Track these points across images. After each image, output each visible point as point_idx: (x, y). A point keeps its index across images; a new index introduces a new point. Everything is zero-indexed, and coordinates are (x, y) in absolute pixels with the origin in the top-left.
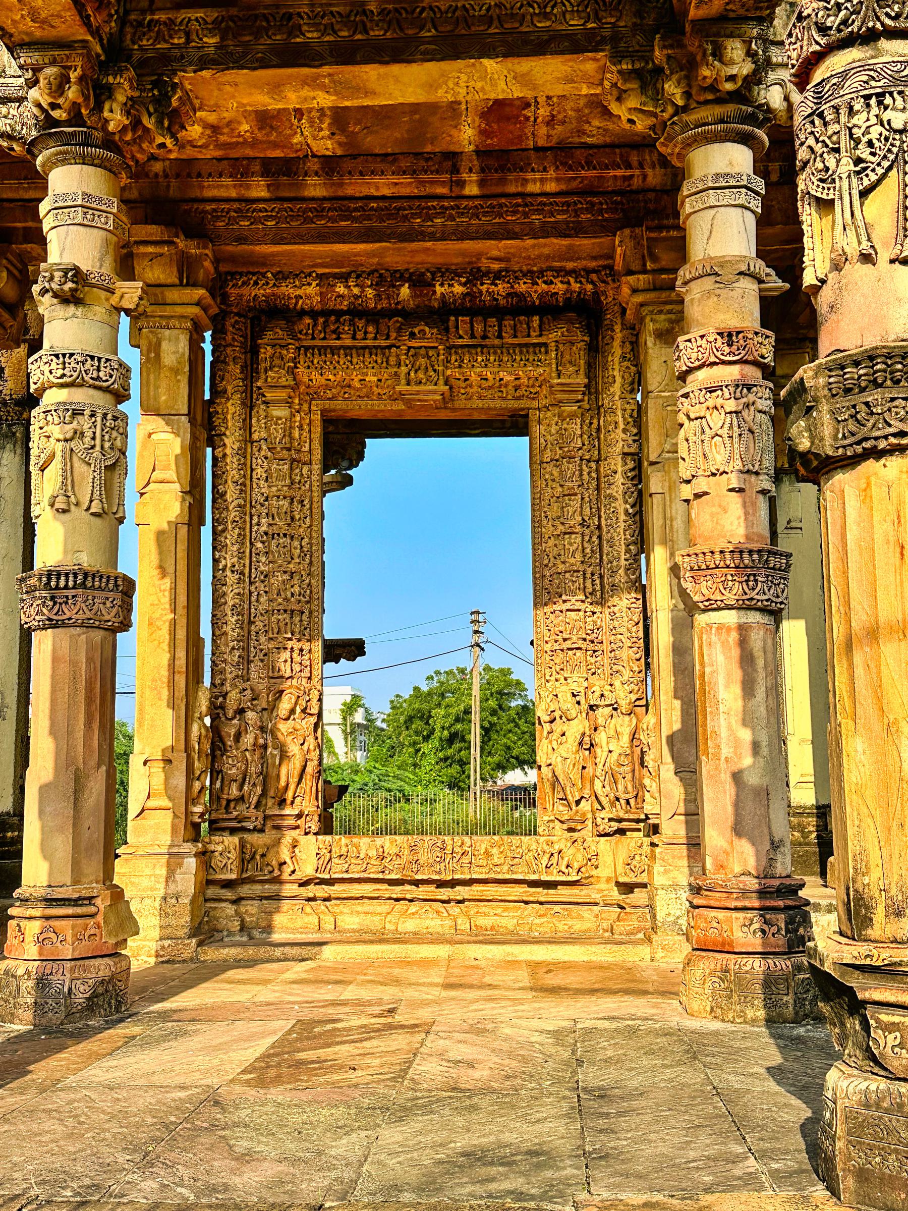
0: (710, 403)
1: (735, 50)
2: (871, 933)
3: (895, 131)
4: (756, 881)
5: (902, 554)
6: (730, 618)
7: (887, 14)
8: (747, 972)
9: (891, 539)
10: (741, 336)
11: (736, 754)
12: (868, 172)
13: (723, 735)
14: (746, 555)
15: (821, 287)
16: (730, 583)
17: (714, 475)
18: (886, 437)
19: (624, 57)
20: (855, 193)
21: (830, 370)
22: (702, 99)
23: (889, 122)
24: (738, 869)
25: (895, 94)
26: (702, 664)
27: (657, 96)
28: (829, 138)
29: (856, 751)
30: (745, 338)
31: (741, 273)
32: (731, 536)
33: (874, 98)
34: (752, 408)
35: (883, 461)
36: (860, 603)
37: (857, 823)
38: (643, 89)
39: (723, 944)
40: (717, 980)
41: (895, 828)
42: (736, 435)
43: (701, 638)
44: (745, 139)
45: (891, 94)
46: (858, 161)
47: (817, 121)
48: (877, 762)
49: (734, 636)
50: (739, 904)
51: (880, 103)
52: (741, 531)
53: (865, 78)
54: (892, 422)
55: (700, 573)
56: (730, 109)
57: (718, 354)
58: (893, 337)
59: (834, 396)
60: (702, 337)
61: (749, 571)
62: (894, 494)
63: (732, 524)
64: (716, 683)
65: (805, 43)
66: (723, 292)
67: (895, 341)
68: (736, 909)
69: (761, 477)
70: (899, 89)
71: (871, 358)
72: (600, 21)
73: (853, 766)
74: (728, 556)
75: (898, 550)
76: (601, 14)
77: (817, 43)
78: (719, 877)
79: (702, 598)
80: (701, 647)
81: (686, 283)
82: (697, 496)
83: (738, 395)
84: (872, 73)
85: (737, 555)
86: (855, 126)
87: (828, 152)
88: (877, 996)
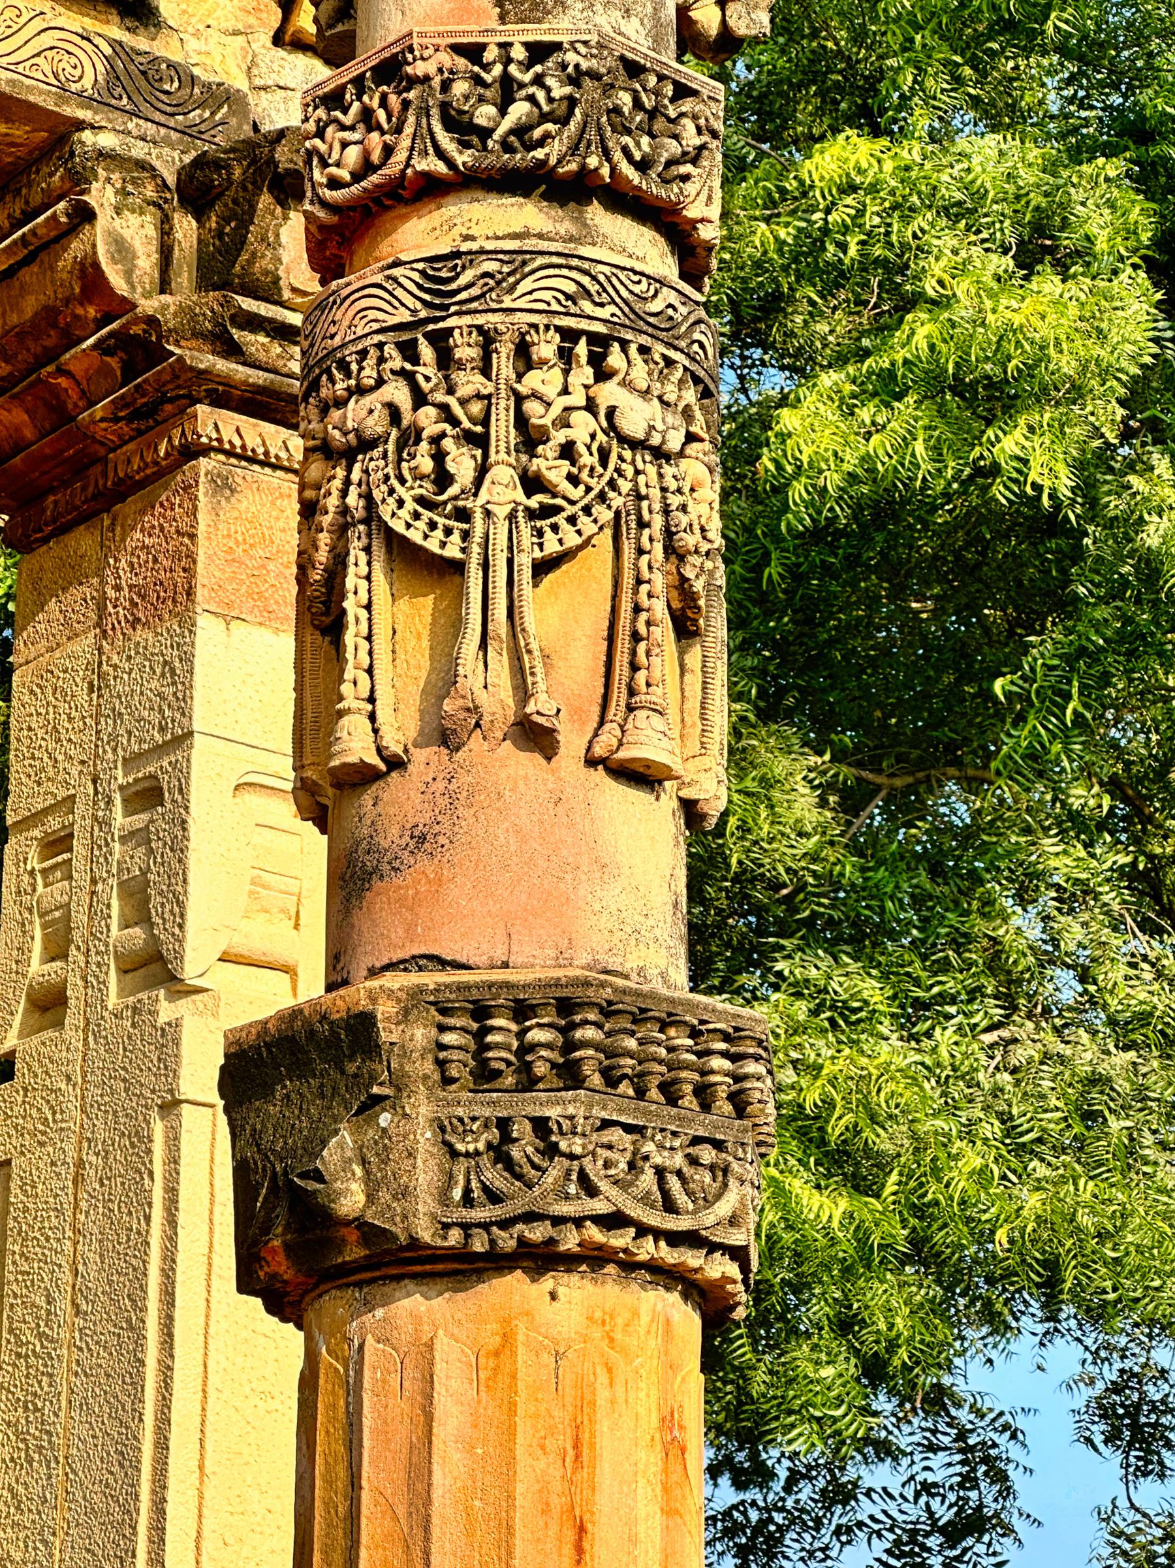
3: (623, 440)
5: (579, 1550)
7: (626, 151)
9: (555, 1501)
12: (560, 519)
18: (578, 1222)
20: (524, 562)
21: (444, 1012)
23: (611, 412)
25: (633, 349)
28: (463, 402)
33: (583, 341)
35: (547, 1283)
45: (624, 344)
46: (532, 483)
47: (426, 352)
51: (597, 361)
53: (571, 288)
54: (603, 1186)
58: (584, 958)
59: (447, 1081)
62: (567, 1379)
65: (406, 143)
67: (588, 967)
70: (644, 340)
71: (566, 1007)
75: (570, 1535)
77: (441, 154)
84: (585, 280)
86: (535, 395)
87: (456, 438)
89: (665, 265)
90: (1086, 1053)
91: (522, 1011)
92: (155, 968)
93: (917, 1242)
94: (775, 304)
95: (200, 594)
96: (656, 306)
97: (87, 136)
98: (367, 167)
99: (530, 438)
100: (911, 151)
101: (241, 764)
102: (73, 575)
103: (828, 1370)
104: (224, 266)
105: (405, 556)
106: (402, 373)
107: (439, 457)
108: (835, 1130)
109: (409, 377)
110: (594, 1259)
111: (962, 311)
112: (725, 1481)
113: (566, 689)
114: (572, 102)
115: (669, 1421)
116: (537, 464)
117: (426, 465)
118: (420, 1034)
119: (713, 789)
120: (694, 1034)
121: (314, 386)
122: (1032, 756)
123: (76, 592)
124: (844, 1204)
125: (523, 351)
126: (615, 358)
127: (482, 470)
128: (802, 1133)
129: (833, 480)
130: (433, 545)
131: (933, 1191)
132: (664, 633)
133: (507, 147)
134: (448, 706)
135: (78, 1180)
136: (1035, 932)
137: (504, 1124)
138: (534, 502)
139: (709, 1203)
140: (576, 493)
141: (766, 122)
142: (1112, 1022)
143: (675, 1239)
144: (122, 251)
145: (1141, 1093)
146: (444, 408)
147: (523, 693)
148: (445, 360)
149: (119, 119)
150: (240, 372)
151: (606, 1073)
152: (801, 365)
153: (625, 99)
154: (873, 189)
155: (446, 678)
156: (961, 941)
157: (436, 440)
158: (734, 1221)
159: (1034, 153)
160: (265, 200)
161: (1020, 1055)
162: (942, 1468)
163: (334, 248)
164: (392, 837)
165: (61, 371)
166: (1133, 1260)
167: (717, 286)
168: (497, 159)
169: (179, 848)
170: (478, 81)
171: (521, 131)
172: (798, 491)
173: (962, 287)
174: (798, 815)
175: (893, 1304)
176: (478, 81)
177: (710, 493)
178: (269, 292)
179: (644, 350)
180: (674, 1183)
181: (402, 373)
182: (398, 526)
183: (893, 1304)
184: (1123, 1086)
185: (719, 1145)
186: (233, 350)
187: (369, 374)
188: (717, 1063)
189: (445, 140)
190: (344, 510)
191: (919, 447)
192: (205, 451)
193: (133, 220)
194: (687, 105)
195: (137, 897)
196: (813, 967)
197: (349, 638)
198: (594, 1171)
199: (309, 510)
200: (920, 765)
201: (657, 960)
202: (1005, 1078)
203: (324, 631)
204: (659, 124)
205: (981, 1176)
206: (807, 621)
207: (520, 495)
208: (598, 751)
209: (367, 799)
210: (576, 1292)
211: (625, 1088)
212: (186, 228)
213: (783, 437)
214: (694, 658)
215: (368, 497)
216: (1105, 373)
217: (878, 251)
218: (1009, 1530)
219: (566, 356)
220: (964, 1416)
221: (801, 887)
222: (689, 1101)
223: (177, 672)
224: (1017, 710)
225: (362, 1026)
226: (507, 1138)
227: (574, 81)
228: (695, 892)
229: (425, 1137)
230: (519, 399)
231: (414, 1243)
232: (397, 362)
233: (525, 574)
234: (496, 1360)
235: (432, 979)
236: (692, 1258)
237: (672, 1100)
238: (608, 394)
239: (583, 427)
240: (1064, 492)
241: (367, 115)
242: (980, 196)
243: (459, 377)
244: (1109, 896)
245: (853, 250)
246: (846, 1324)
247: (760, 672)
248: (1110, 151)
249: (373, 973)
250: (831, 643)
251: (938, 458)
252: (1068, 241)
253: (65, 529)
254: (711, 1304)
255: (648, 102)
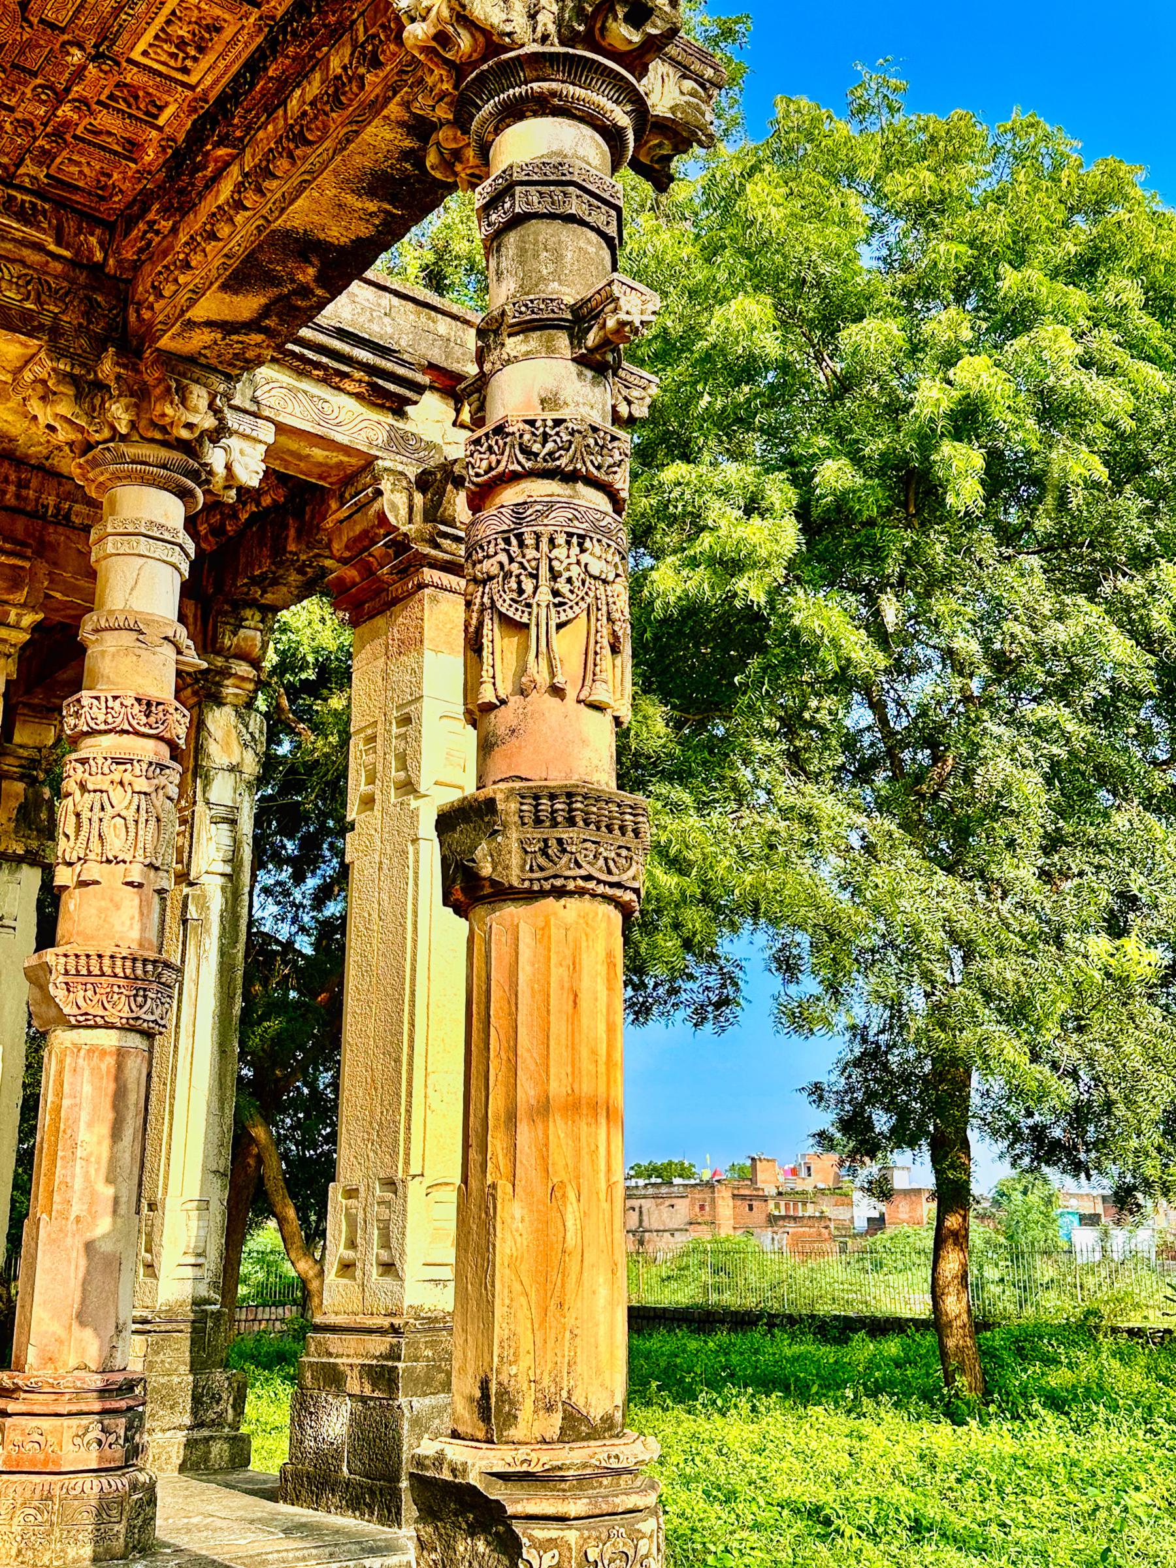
0: (116, 777)
1: (199, 396)
2: (513, 1433)
4: (99, 1377)
5: (575, 1003)
6: (109, 1039)
8: (75, 1498)
10: (161, 708)
11: (89, 1212)
13: (76, 1187)
14: (139, 965)
15: (496, 707)
16: (116, 997)
17: (109, 861)
18: (574, 878)
19: (63, 356)
20: (553, 624)
22: (149, 435)
24: (73, 1362)
26: (59, 1094)
27: (93, 413)
29: (513, 1218)
30: (165, 712)
31: (166, 638)
32: (121, 938)
34: (161, 792)
35: (563, 901)
36: (529, 1050)
37: (507, 1302)
38: (78, 398)
39: (46, 1462)
40: (33, 1511)
41: (552, 1307)
42: (142, 820)
43: (61, 1062)
44: (184, 494)
46: (556, 593)
47: (514, 541)
48: (537, 1230)
49: (111, 1061)
50: (74, 1408)
51: (580, 545)
52: (135, 934)
55: (80, 979)
56: (176, 456)
57: (134, 723)
58: (576, 777)
59: (524, 824)
60: (115, 698)
61: (139, 984)
62: (570, 938)
63: (123, 924)
64: (77, 1121)
65: (505, 458)
66: (143, 653)
68: (70, 1414)
69: (161, 873)
71: (569, 795)
72: (42, 304)
73: (508, 1236)
74: (119, 962)
75: (571, 998)
76: (43, 297)
77: (519, 463)
78: (47, 1374)
79: (76, 1011)
80: (60, 1072)
81: (97, 631)
82: (83, 884)
83: (150, 774)
85: (128, 963)
88: (532, 1508)
89: (607, 507)
90: (770, 821)
91: (552, 797)
92: (408, 787)
93: (704, 894)
94: (649, 530)
95: (426, 642)
96: (603, 523)
97: (380, 462)
98: (490, 469)
99: (555, 576)
100: (703, 469)
101: (443, 708)
102: (375, 635)
103: (669, 943)
104: (433, 513)
105: (508, 623)
106: (504, 550)
107: (519, 583)
108: (672, 852)
109: (507, 551)
110: (581, 892)
111: (722, 532)
112: (629, 988)
113: (569, 674)
114: (571, 442)
115: (610, 955)
116: (557, 586)
117: (515, 586)
118: (514, 806)
119: (626, 714)
120: (619, 806)
121: (470, 555)
122: (749, 706)
123: (377, 641)
124: (676, 879)
125: (552, 541)
126: (588, 544)
127: (536, 588)
128: (660, 852)
129: (672, 599)
130: (517, 618)
131: (710, 874)
132: (607, 651)
133: (545, 460)
134: (524, 680)
135: (380, 869)
136: (751, 777)
137: (545, 841)
138: (556, 600)
139: (625, 871)
140: (572, 597)
141: (645, 456)
142: (780, 810)
143: (612, 885)
144: (394, 507)
145: (791, 838)
146: (521, 563)
147: (553, 674)
148: (521, 545)
149: (392, 456)
150: (441, 555)
151: (585, 820)
152: (658, 555)
153: (591, 442)
154: (688, 484)
155: (523, 670)
156: (722, 778)
157: (518, 576)
158: (634, 878)
159: (751, 469)
160: (450, 487)
161: (744, 823)
162: (713, 981)
163: (477, 502)
164: (502, 731)
165: (370, 555)
166: (787, 901)
167: (629, 515)
168: (541, 465)
169: (417, 740)
170: (534, 434)
171: (550, 454)
172: (658, 604)
173: (723, 523)
174: (656, 728)
175: (694, 918)
176: (534, 434)
177: (625, 596)
178: (451, 523)
179: (599, 541)
180: (611, 864)
181: (504, 550)
182: (503, 610)
183: (694, 918)
184: (784, 834)
185: (628, 849)
186: (437, 546)
187: (491, 551)
188: (628, 817)
189: (521, 457)
190: (482, 604)
191: (706, 586)
192: (427, 586)
193: (398, 495)
194: (616, 444)
195: (402, 759)
196: (663, 788)
197: (485, 654)
198: (580, 858)
199: (468, 604)
200: (705, 710)
201: (605, 778)
202: (738, 831)
203: (475, 651)
204: (605, 451)
205: (729, 868)
206: (661, 655)
207: (551, 597)
208: (582, 697)
209: (492, 716)
210: (573, 905)
211: (592, 826)
212: (418, 498)
213: (652, 582)
214: (618, 662)
215: (492, 599)
216: (779, 556)
217: (690, 509)
218: (739, 1004)
219: (568, 543)
220: (722, 962)
221: (659, 758)
222: (617, 832)
223: (417, 673)
224: (744, 689)
225: (491, 803)
226: (547, 846)
227: (572, 434)
228: (619, 761)
229: (515, 846)
230: (551, 560)
231: (511, 887)
232: (503, 546)
233: (553, 629)
234: (542, 933)
235: (518, 785)
236: (618, 892)
237: (610, 831)
238: (585, 558)
239: (575, 571)
240: (763, 604)
241: (490, 448)
242: (730, 487)
243: (527, 551)
244: (778, 761)
245: (680, 509)
246: (677, 926)
247: (643, 675)
248: (780, 469)
249: (494, 783)
250: (670, 665)
251: (713, 589)
252: (764, 504)
253: (371, 617)
254: (625, 910)
255: (601, 442)
